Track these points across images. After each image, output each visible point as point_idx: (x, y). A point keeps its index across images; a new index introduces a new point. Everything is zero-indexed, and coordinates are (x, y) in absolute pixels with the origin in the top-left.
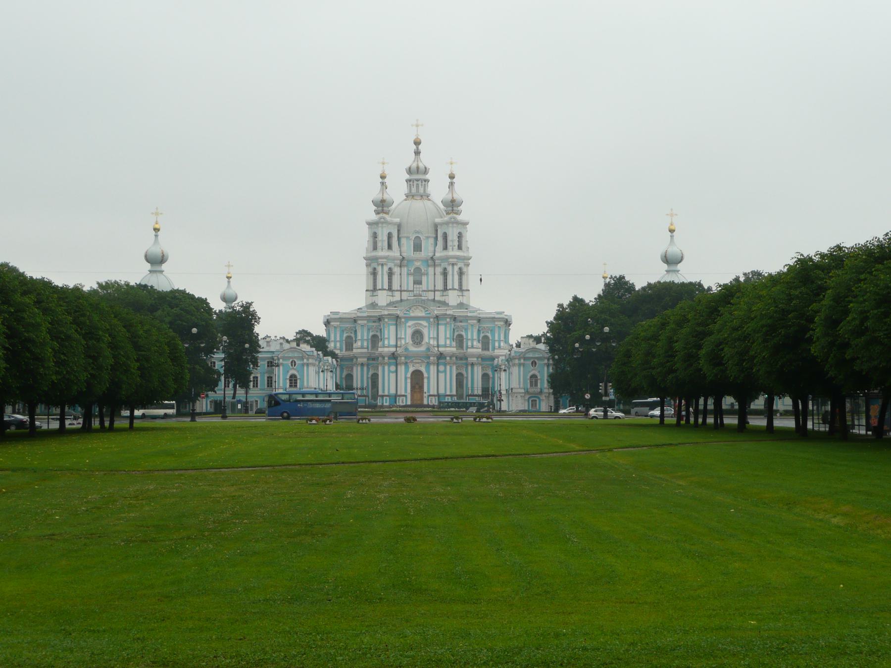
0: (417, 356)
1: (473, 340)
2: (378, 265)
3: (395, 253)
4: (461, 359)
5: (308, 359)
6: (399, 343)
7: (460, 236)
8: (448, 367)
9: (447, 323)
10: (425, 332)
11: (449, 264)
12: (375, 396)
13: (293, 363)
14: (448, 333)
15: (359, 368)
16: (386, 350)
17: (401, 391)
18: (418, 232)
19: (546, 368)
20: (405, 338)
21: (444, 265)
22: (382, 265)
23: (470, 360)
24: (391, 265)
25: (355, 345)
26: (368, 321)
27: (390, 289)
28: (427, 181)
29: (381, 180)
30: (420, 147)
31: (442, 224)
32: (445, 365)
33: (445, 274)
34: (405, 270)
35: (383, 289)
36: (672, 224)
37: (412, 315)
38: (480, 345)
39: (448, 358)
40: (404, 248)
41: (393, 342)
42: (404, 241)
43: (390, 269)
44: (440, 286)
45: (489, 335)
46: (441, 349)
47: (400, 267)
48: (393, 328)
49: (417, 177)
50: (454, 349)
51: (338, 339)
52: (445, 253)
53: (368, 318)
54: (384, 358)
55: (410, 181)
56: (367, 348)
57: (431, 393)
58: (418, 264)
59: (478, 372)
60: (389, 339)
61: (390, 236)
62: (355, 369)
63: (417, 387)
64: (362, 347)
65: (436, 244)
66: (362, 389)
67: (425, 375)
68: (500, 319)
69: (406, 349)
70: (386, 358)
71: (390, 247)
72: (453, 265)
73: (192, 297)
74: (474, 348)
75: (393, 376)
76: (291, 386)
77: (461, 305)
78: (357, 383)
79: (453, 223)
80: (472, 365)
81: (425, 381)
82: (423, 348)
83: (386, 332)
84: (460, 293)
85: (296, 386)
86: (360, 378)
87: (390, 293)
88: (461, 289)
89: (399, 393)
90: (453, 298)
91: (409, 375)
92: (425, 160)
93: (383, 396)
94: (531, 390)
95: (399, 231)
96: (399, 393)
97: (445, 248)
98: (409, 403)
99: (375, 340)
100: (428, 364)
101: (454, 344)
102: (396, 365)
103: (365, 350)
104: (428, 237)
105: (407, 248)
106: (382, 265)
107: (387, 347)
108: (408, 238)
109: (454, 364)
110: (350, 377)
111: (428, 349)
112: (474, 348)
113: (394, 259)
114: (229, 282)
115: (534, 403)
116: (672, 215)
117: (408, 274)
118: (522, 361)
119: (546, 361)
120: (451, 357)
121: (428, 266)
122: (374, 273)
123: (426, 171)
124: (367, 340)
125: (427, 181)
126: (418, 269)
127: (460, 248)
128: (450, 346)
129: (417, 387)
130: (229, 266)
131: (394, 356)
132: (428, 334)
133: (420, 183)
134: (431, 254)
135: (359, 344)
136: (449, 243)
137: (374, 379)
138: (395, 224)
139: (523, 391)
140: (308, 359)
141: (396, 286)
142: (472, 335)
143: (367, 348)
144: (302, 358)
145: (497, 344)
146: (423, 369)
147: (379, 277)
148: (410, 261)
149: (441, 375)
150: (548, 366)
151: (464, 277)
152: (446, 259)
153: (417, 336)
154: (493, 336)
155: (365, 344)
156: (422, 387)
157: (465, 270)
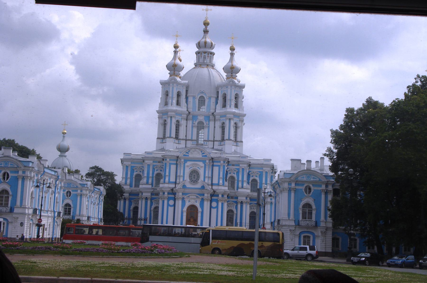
2: (226, 119)
3: (183, 108)
4: (232, 198)
6: (178, 181)
8: (220, 204)
10: (201, 172)
15: (144, 201)
16: (166, 185)
18: (202, 92)
19: (323, 196)
22: (230, 119)
23: (240, 199)
24: (178, 118)
27: (177, 137)
28: (213, 54)
30: (209, 28)
32: (217, 201)
33: (223, 128)
34: (190, 123)
35: (170, 137)
38: (249, 186)
39: (220, 196)
40: (191, 105)
41: (173, 179)
42: (190, 99)
43: (178, 121)
44: (218, 137)
46: (215, 187)
47: (187, 120)
48: (173, 167)
51: (129, 176)
52: (224, 110)
54: (164, 193)
58: (201, 118)
59: (247, 210)
61: (179, 95)
62: (140, 202)
63: (192, 220)
64: (147, 183)
65: (217, 103)
67: (200, 210)
68: (267, 166)
69: (184, 186)
70: (166, 193)
71: (178, 104)
74: (245, 190)
75: (171, 209)
77: (235, 152)
78: (141, 214)
80: (242, 203)
81: (199, 215)
82: (199, 186)
84: (235, 144)
87: (177, 141)
88: (236, 141)
90: (229, 148)
91: (185, 209)
95: (187, 91)
101: (226, 183)
102: (175, 200)
115: (306, 240)
117: (192, 127)
122: (165, 124)
125: (213, 54)
126: (201, 123)
127: (236, 106)
128: (223, 185)
129: (192, 220)
131: (173, 192)
133: (206, 55)
134: (212, 111)
136: (228, 103)
138: (183, 85)
139: (293, 223)
141: (182, 135)
145: (240, 185)
146: (198, 205)
149: (214, 211)
150: (326, 193)
151: (239, 131)
152: (223, 116)
155: (150, 181)
157: (239, 124)
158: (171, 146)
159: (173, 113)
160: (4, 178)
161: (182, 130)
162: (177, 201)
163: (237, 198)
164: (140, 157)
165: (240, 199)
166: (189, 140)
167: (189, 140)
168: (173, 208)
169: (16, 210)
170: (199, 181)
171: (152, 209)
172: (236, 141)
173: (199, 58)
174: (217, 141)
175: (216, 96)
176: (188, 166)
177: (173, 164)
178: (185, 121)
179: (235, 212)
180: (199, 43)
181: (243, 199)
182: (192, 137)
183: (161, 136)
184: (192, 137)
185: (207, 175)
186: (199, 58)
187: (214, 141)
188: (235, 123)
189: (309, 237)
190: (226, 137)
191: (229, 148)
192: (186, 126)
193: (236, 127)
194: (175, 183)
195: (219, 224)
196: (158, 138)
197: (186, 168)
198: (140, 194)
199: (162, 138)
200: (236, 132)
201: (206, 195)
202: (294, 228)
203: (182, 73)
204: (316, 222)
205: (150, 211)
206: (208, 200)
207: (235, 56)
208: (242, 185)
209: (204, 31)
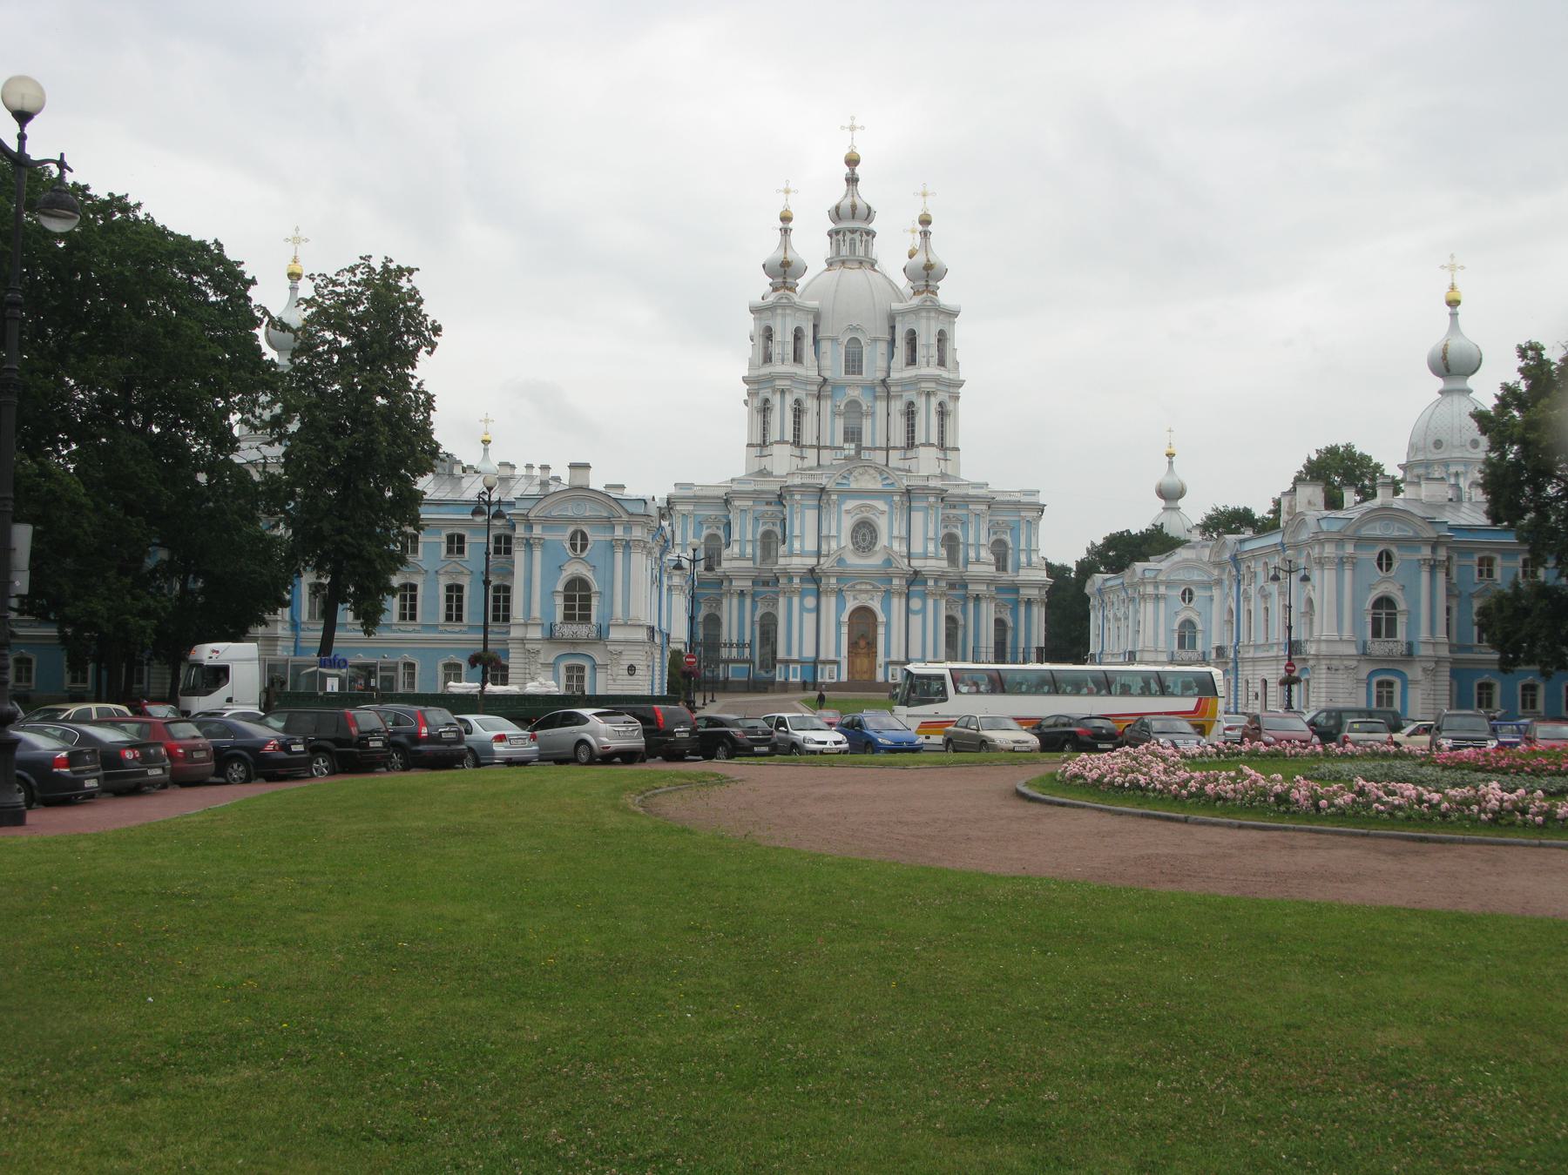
0: (862, 576)
1: (978, 546)
2: (774, 392)
5: (628, 527)
6: (824, 548)
7: (942, 338)
8: (930, 602)
9: (930, 506)
10: (882, 523)
11: (919, 394)
12: (771, 661)
13: (579, 541)
14: (931, 527)
15: (735, 601)
16: (796, 561)
17: (828, 652)
18: (855, 329)
19: (1425, 576)
20: (838, 537)
21: (910, 395)
22: (783, 392)
23: (974, 588)
24: (799, 393)
25: (725, 553)
26: (755, 500)
27: (797, 442)
29: (780, 224)
30: (858, 170)
31: (904, 313)
33: (910, 413)
34: (827, 405)
36: (1453, 288)
37: (854, 486)
39: (931, 583)
40: (826, 362)
41: (811, 545)
42: (825, 346)
43: (797, 401)
44: (899, 438)
45: (1008, 538)
46: (915, 563)
47: (819, 398)
49: (851, 227)
50: (944, 564)
52: (911, 372)
53: (756, 496)
54: (791, 579)
55: (837, 233)
56: (753, 559)
57: (894, 658)
58: (854, 393)
59: (988, 613)
60: (802, 537)
61: (798, 336)
62: (725, 602)
63: (862, 643)
64: (742, 557)
66: (741, 645)
67: (881, 618)
69: (840, 561)
70: (796, 580)
71: (797, 358)
72: (928, 394)
73: (162, 233)
74: (982, 565)
75: (810, 619)
76: (569, 618)
77: (944, 476)
78: (730, 630)
79: (928, 310)
80: (977, 598)
81: (881, 630)
82: (875, 560)
83: (797, 523)
85: (586, 618)
86: (736, 622)
88: (942, 446)
89: (822, 657)
90: (926, 463)
91: (845, 618)
92: (867, 193)
93: (787, 662)
94: (1379, 648)
95: (815, 326)
96: (822, 657)
97: (912, 361)
98: (844, 677)
99: (768, 542)
100: (888, 594)
103: (750, 564)
104: (875, 340)
105: (833, 363)
106: (783, 392)
107: (797, 556)
108: (834, 340)
109: (943, 595)
110: (714, 621)
111: (888, 562)
112: (982, 565)
113: (807, 382)
114: (486, 450)
116: (1452, 268)
117: (834, 414)
118: (1349, 549)
119: (1426, 552)
120: (936, 581)
121: (875, 398)
122: (765, 409)
123: (869, 214)
124: (753, 541)
127: (942, 362)
129: (862, 643)
130: (486, 421)
131: (813, 576)
132: (888, 529)
133: (857, 236)
134: (881, 375)
135: (735, 549)
136: (921, 352)
137: (768, 629)
140: (628, 527)
141: (808, 437)
142: (978, 537)
143: (753, 559)
144: (609, 523)
145: (1023, 559)
146: (876, 605)
147: (775, 418)
148: (838, 387)
149: (916, 621)
150: (1433, 569)
151: (949, 422)
153: (865, 533)
154: (1017, 540)
155: (749, 550)
156: (872, 645)
157: (950, 406)
158: (782, 461)
159: (933, 385)
160: (574, 546)
161: (809, 422)
162: (823, 599)
163: (965, 586)
164: (721, 492)
165: (1025, 593)
166: (826, 447)
167: (826, 447)
168: (814, 615)
169: (614, 634)
170: (877, 548)
171: (757, 618)
172: (942, 446)
173: (838, 246)
174: (895, 448)
175: (888, 337)
176: (848, 512)
177: (809, 507)
178: (815, 402)
179: (961, 622)
180: (837, 208)
181: (981, 588)
182: (873, 440)
183: (758, 440)
184: (873, 440)
185: (896, 533)
186: (838, 246)
187: (887, 449)
188: (940, 404)
189: (582, 669)
190: (920, 437)
191: (926, 463)
192: (818, 414)
193: (943, 413)
194: (819, 554)
195: (657, 687)
196: (749, 445)
197: (844, 516)
198: (725, 583)
199: (762, 445)
200: (942, 426)
201: (896, 582)
202: (1354, 663)
203: (802, 282)
204: (1410, 645)
205: (753, 623)
206: (900, 594)
207: (793, 236)
208: (978, 554)
209: (847, 180)
